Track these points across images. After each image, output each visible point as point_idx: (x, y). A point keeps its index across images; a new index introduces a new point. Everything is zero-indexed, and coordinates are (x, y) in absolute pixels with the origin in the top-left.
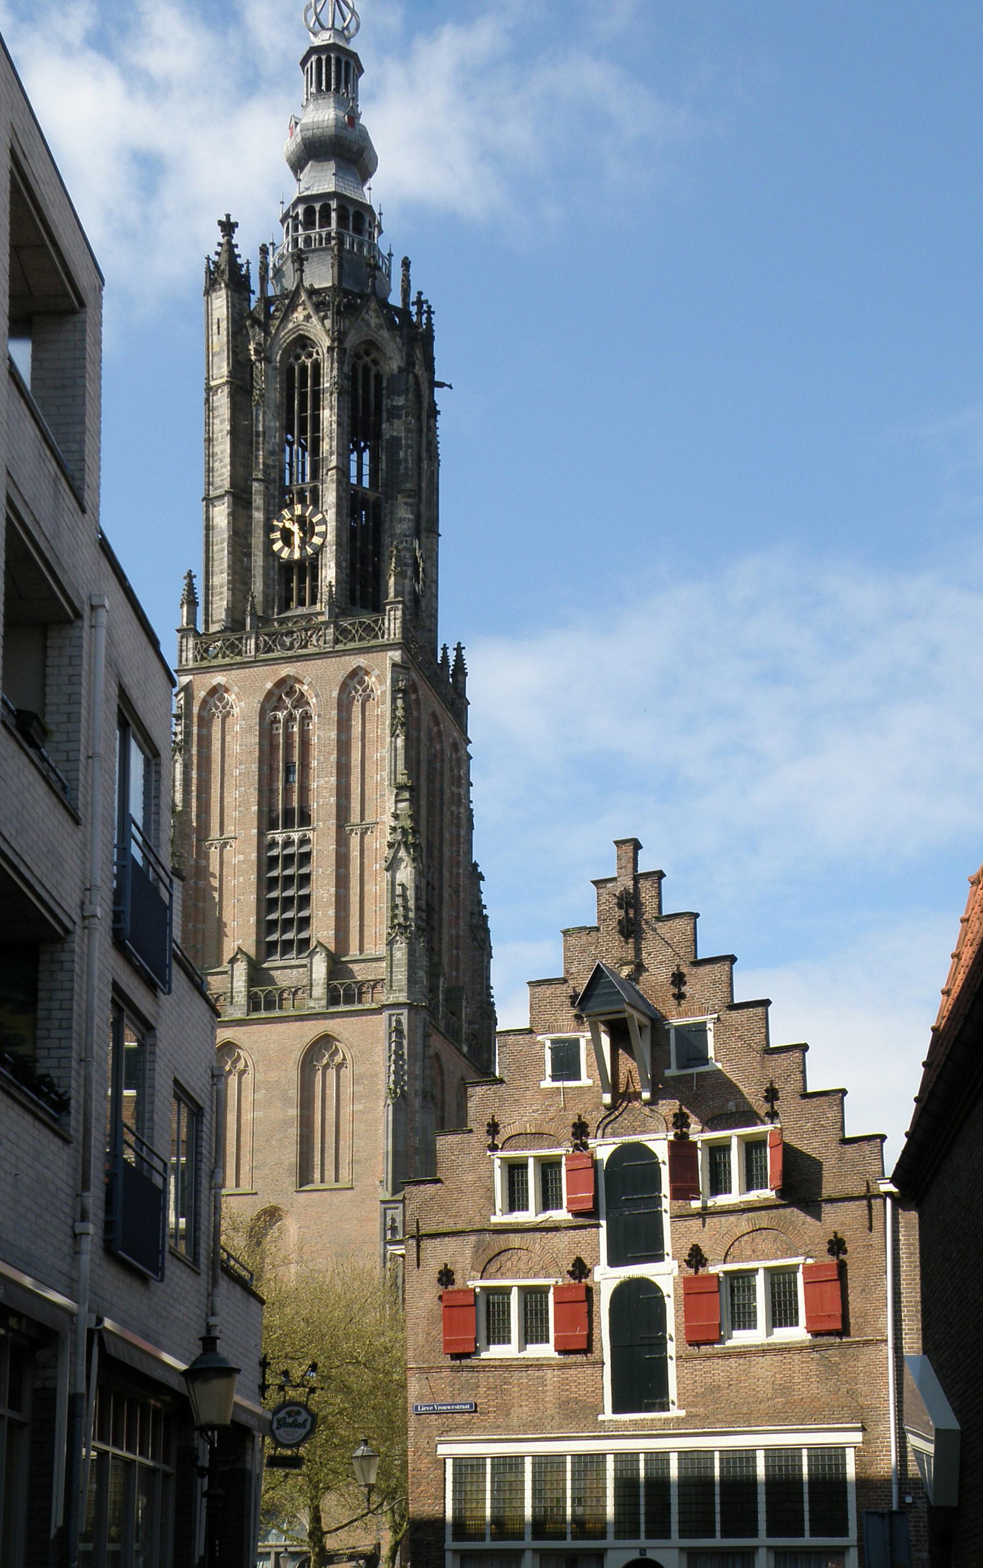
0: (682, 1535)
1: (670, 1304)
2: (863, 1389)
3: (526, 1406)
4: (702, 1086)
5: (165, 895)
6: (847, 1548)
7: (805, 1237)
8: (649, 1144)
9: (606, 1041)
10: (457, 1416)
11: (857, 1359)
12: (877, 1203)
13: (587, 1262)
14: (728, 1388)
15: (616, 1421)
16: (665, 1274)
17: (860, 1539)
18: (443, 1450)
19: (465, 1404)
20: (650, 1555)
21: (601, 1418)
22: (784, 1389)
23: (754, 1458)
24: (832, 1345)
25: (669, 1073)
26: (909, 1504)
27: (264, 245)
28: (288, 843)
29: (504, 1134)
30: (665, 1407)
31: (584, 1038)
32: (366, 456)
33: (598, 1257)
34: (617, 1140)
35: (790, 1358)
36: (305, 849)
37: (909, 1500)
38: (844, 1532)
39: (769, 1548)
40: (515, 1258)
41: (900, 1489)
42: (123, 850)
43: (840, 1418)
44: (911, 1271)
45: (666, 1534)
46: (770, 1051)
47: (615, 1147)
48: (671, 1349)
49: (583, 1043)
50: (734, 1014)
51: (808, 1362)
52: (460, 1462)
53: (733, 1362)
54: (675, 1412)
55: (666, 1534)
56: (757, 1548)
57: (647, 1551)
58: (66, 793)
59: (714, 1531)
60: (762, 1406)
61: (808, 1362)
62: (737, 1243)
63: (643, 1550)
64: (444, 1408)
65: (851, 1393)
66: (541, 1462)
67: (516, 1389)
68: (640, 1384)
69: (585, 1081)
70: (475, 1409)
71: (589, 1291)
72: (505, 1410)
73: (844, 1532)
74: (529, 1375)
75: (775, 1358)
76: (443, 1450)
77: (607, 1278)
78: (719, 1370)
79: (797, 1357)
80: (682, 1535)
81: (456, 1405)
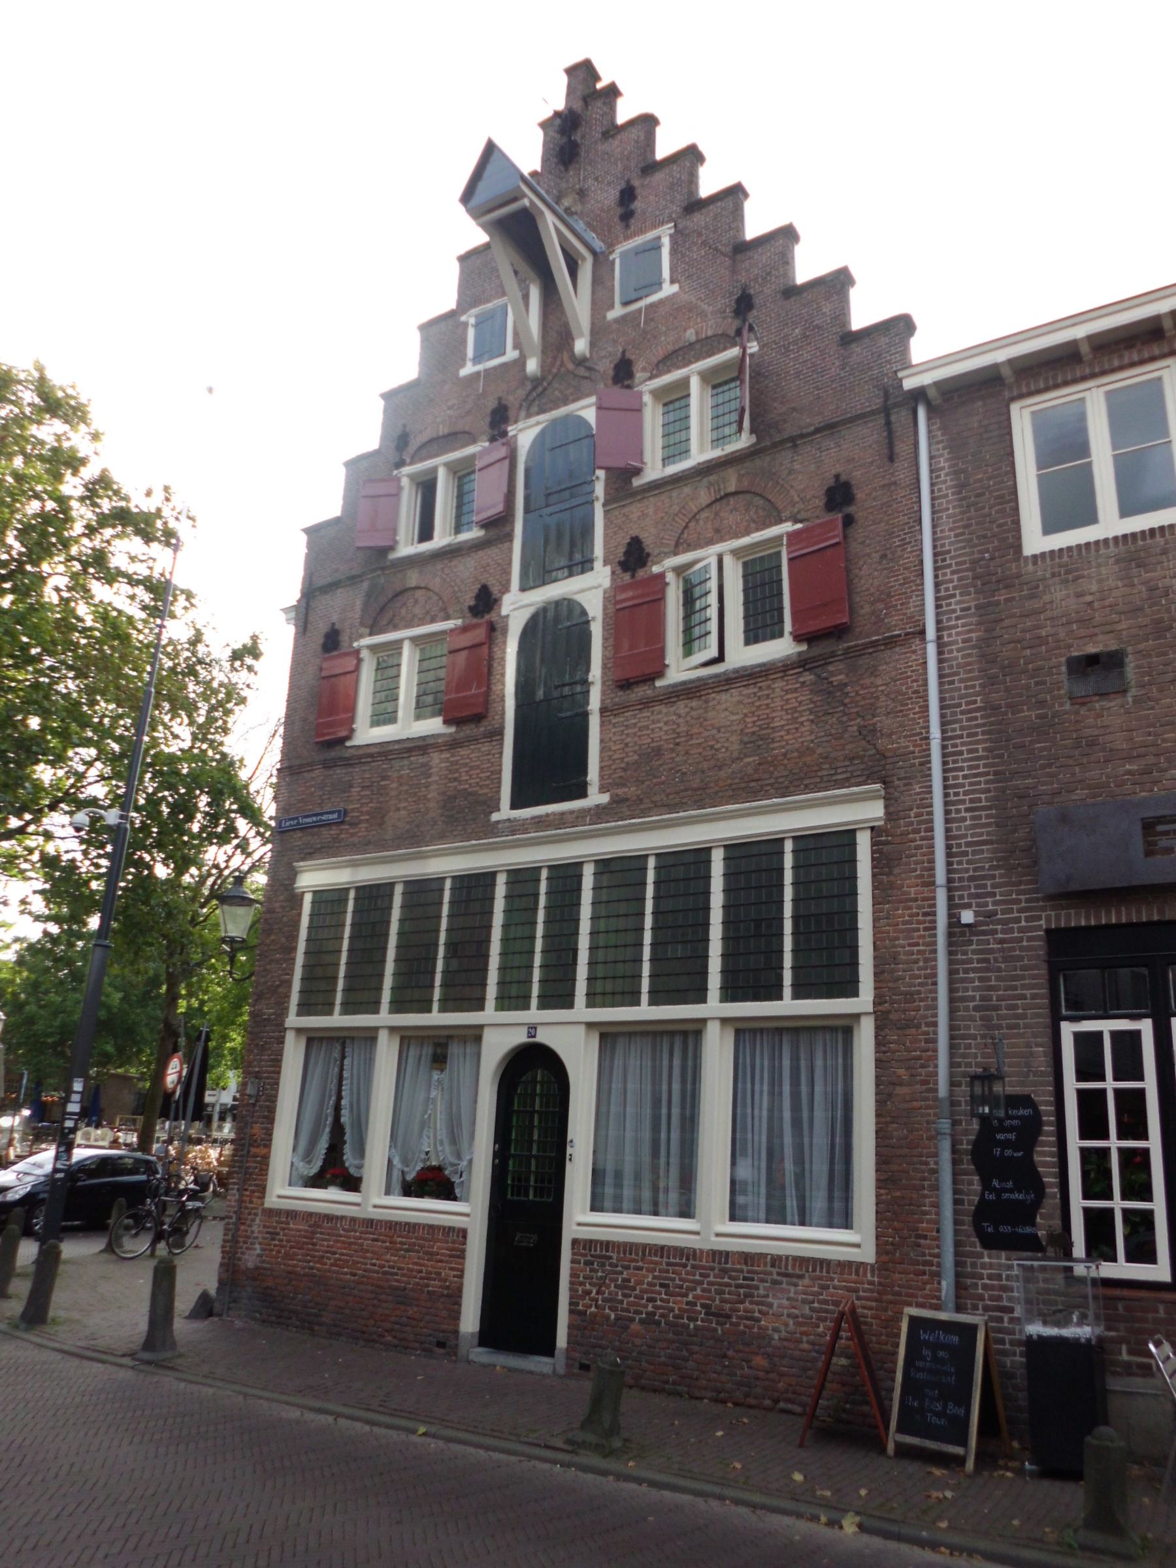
0: (593, 1000)
2: (884, 722)
3: (405, 808)
4: (652, 320)
5: (269, 854)
6: (857, 1017)
7: (792, 492)
10: (324, 831)
11: (874, 672)
12: (900, 417)
13: (495, 590)
14: (672, 750)
15: (515, 820)
17: (878, 1000)
19: (332, 813)
20: (542, 1037)
21: (495, 817)
22: (757, 741)
23: (708, 862)
24: (833, 654)
25: (612, 315)
26: (968, 925)
29: (414, 443)
30: (583, 794)
33: (509, 581)
35: (769, 687)
37: (967, 917)
38: (849, 988)
39: (725, 1021)
40: (410, 602)
41: (950, 898)
43: (847, 779)
44: (962, 513)
45: (566, 1001)
48: (595, 702)
51: (795, 690)
53: (682, 707)
54: (596, 797)
55: (566, 1001)
56: (704, 1021)
57: (540, 1030)
58: (169, 538)
59: (780, 986)
60: (722, 774)
61: (795, 690)
62: (692, 524)
63: (532, 1029)
64: (309, 820)
65: (868, 733)
67: (394, 785)
70: (343, 818)
71: (492, 628)
72: (378, 817)
73: (849, 988)
74: (412, 763)
75: (746, 692)
78: (660, 723)
79: (779, 684)
80: (593, 1000)
81: (322, 814)
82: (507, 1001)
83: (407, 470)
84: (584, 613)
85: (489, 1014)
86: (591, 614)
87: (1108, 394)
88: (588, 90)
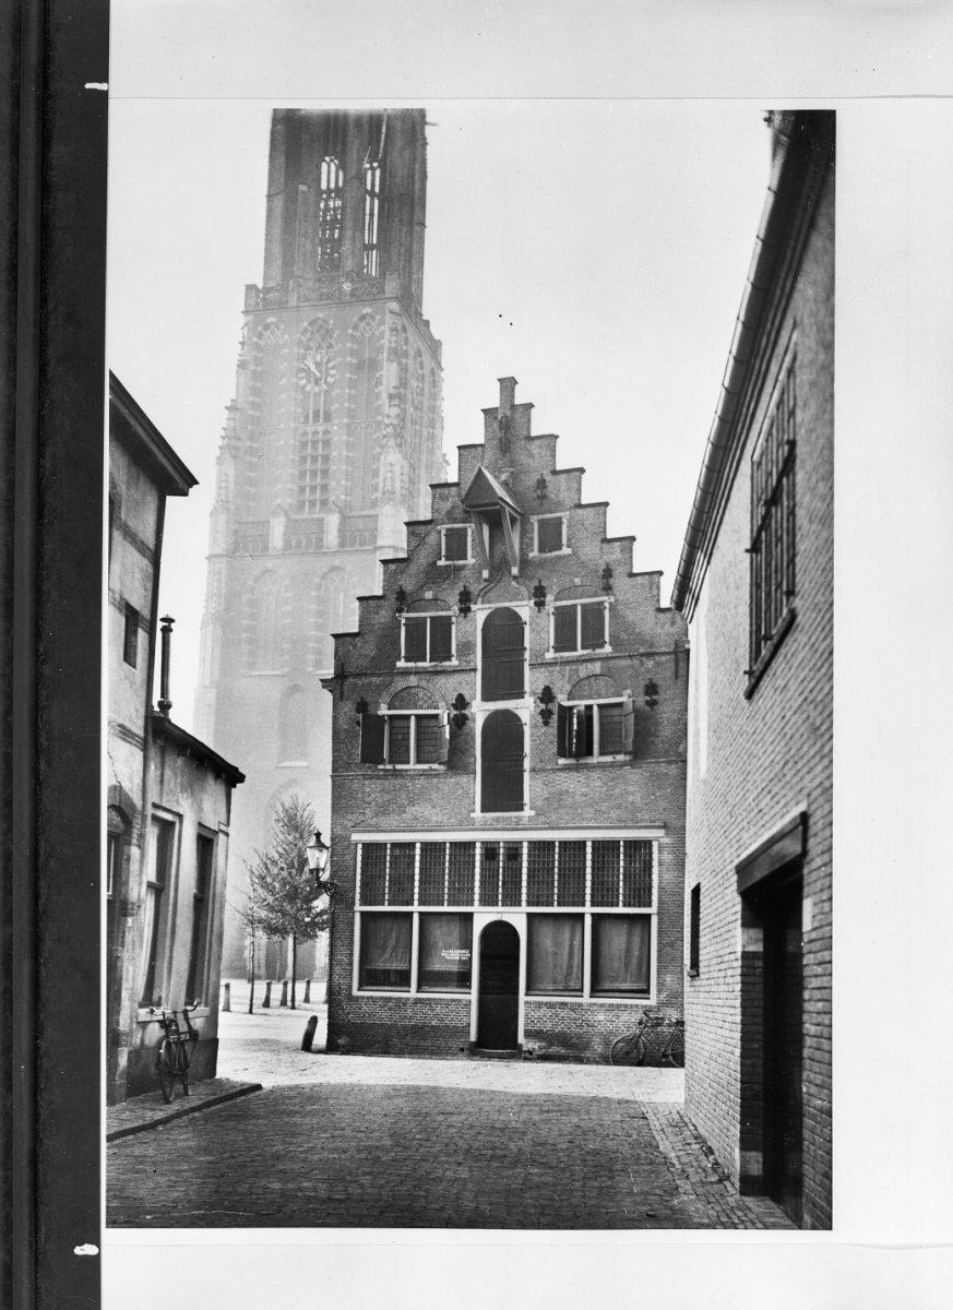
0: (529, 904)
1: (527, 730)
8: (516, 609)
9: (486, 529)
13: (467, 697)
16: (525, 709)
17: (659, 908)
18: (355, 837)
27: (657, 693)
28: (316, 433)
31: (470, 528)
32: (378, 172)
34: (492, 606)
36: (326, 437)
38: (649, 905)
42: (623, 764)
46: (606, 541)
47: (490, 611)
48: (527, 764)
49: (469, 532)
50: (580, 511)
52: (367, 847)
54: (528, 812)
66: (536, 846)
68: (503, 792)
69: (470, 561)
73: (649, 905)
76: (355, 837)
77: (480, 711)
82: (485, 901)
83: (405, 615)
84: (519, 720)
85: (476, 908)
86: (523, 722)
87: (112, 1223)
88: (531, 406)
